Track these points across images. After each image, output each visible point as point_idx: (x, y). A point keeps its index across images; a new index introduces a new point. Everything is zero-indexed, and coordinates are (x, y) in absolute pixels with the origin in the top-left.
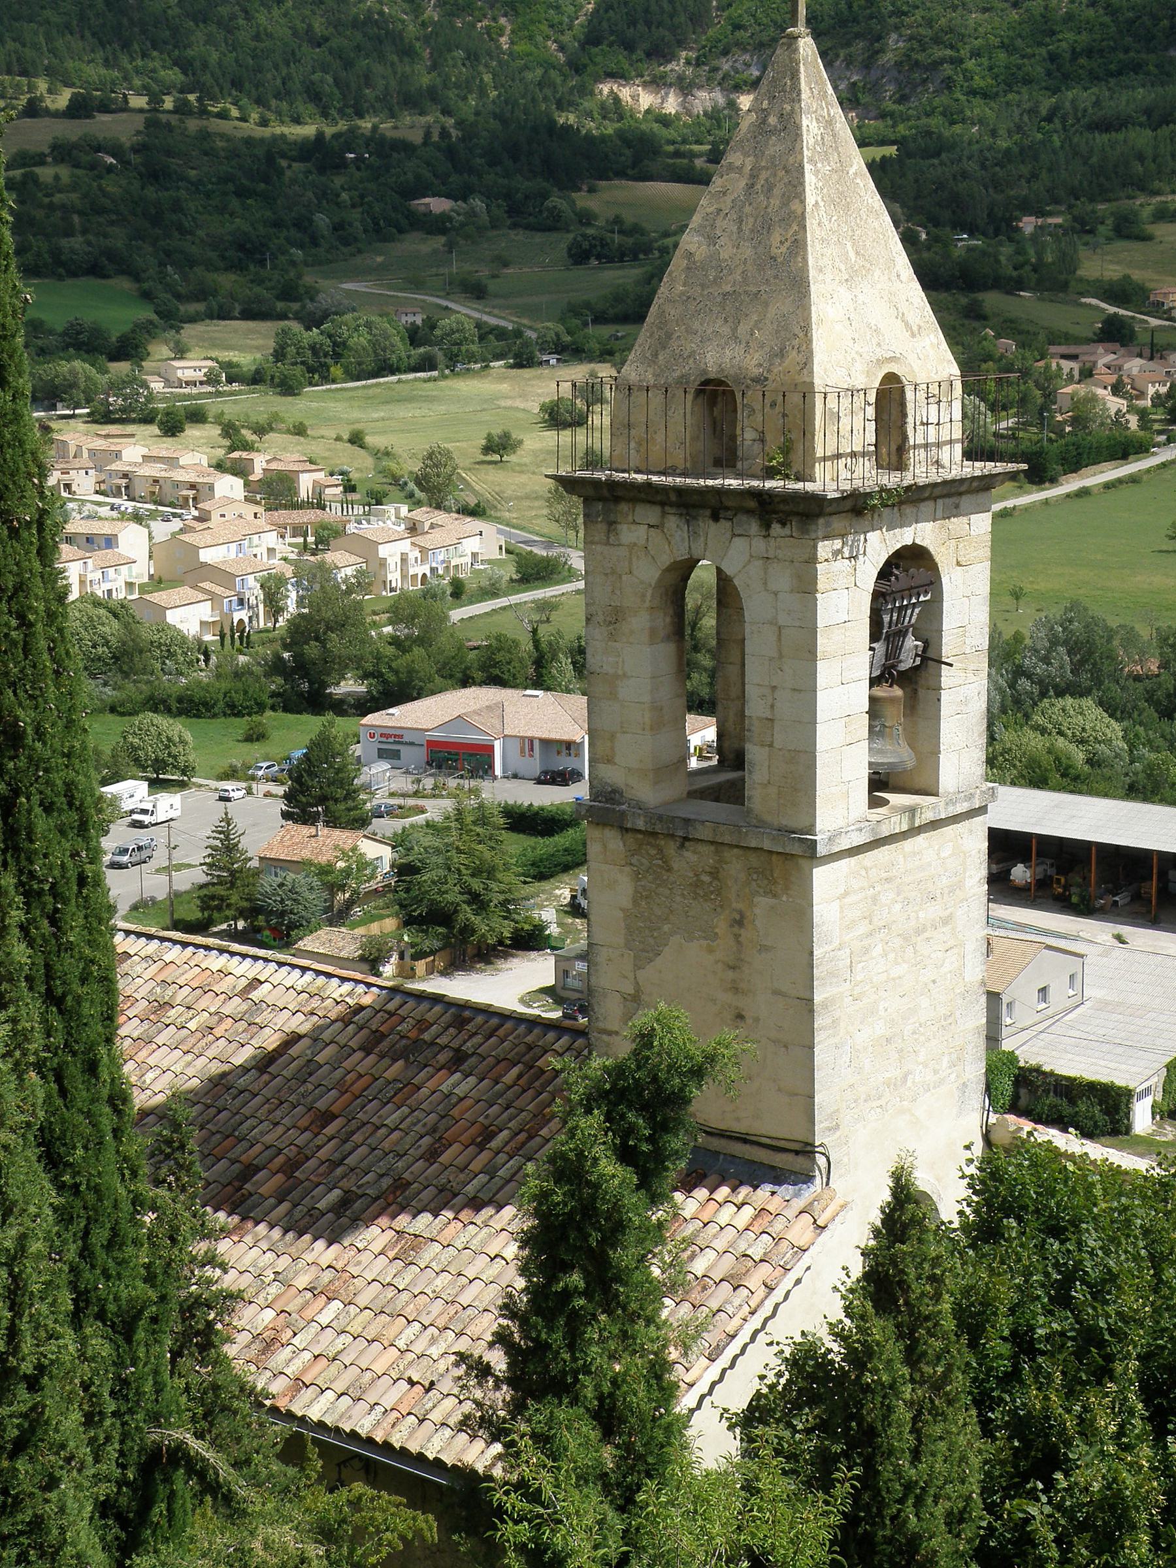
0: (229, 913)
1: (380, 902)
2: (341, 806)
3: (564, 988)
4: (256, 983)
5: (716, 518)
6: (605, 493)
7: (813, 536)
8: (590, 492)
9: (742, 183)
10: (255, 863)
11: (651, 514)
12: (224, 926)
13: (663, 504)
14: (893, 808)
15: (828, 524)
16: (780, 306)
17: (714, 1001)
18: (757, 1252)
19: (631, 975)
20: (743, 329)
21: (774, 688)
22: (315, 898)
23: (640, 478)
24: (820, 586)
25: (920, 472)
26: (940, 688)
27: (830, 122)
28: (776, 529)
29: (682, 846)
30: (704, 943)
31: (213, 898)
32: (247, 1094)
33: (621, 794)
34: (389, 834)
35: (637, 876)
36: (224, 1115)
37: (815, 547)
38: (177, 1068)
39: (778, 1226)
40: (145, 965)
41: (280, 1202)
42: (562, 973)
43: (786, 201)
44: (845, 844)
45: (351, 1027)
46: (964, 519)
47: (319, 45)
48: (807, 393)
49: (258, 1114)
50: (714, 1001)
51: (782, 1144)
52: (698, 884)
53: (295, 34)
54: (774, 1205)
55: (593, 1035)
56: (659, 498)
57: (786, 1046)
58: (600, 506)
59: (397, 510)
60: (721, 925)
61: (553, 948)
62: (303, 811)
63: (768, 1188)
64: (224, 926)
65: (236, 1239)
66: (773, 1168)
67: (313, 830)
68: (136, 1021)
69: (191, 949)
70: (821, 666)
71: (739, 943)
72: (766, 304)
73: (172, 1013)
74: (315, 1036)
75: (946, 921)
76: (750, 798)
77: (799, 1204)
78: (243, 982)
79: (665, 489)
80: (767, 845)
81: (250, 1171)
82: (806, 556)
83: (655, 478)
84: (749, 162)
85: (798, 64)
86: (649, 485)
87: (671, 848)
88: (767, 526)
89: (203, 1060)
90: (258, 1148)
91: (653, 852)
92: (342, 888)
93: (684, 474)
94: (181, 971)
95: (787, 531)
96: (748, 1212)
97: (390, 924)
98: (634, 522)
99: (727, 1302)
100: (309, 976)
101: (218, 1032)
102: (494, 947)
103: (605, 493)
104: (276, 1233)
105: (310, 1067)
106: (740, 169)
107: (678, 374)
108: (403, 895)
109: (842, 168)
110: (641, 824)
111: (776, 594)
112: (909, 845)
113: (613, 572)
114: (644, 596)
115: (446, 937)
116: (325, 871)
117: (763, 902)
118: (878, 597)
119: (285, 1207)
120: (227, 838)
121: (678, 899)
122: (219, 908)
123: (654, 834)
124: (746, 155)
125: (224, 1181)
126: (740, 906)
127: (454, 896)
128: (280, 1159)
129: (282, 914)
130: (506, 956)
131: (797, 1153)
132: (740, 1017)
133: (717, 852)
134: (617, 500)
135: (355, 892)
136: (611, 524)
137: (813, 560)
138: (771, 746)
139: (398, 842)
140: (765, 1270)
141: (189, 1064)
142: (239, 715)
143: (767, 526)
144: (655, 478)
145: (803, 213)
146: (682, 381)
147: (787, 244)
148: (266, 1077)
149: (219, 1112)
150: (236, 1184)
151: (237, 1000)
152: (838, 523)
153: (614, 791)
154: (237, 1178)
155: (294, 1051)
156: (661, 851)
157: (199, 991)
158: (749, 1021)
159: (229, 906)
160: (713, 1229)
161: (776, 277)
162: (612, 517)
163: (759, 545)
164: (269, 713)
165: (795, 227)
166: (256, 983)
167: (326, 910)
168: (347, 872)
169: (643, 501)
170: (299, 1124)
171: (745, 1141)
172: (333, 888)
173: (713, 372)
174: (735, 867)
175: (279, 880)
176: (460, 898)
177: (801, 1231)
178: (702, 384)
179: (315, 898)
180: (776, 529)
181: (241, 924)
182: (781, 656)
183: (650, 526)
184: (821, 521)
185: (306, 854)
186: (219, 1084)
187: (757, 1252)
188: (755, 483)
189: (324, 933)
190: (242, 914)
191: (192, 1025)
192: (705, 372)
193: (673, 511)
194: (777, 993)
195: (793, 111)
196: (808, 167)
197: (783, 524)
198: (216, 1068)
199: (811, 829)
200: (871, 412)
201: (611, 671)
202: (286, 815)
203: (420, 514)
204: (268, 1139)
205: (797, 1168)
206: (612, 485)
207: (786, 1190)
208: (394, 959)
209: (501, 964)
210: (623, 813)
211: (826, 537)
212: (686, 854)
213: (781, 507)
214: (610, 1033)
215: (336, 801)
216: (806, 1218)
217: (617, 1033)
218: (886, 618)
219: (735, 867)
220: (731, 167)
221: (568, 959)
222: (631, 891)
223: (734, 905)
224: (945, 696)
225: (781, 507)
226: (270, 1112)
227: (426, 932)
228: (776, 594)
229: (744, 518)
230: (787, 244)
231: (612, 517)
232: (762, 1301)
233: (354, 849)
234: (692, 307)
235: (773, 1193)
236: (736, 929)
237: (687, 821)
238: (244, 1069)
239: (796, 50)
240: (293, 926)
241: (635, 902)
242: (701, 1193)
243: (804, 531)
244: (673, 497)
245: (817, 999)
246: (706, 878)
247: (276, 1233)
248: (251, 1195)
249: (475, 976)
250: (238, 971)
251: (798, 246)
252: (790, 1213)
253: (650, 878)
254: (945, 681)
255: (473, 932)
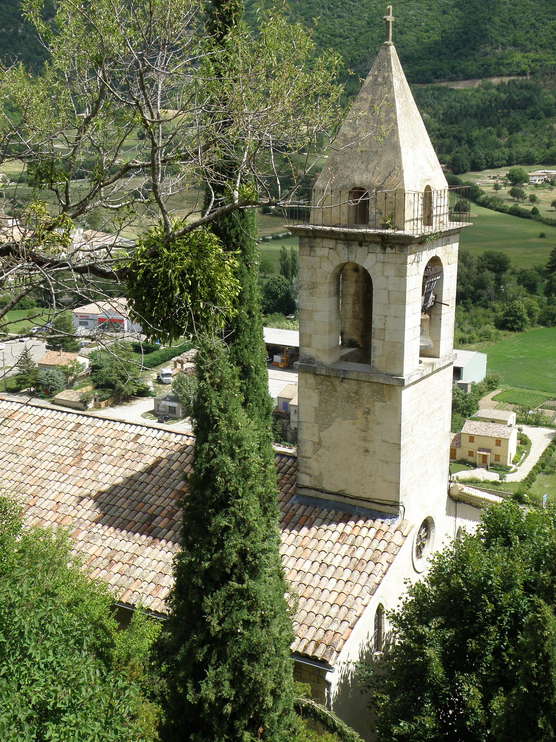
0: (29, 385)
1: (86, 380)
2: (69, 344)
3: (158, 411)
4: (139, 436)
5: (361, 245)
6: (311, 234)
7: (406, 253)
8: (303, 234)
9: (368, 106)
10: (37, 366)
11: (332, 243)
12: (26, 390)
13: (336, 239)
14: (425, 364)
15: (411, 248)
16: (387, 157)
17: (355, 445)
18: (382, 547)
19: (317, 434)
20: (371, 166)
21: (386, 316)
22: (61, 379)
23: (328, 228)
24: (408, 274)
25: (435, 227)
26: (441, 314)
27: (402, 81)
28: (388, 250)
29: (342, 381)
30: (351, 421)
31: (21, 379)
32: (144, 484)
33: (314, 360)
34: (87, 354)
35: (321, 394)
36: (136, 493)
37: (406, 258)
38: (112, 473)
39: (388, 537)
40: (88, 428)
41: (169, 530)
42: (157, 405)
43: (388, 113)
44: (413, 380)
45: (184, 454)
46: (450, 245)
47: (40, 55)
48: (403, 193)
49: (170, 496)
50: (355, 445)
51: (385, 502)
52: (349, 397)
53: (30, 50)
54: (384, 527)
55: (299, 459)
56: (336, 237)
57: (387, 463)
58: (307, 240)
59: (79, 231)
60: (359, 414)
61: (152, 396)
62: (54, 346)
63: (380, 520)
64: (26, 390)
65: (153, 546)
66: (380, 512)
67: (59, 353)
68: (89, 453)
69: (107, 422)
70: (407, 307)
71: (367, 421)
72: (381, 156)
73: (105, 449)
74: (169, 458)
75: (440, 408)
76: (373, 361)
77: (394, 527)
78: (133, 436)
79: (339, 233)
80: (382, 381)
81: (152, 517)
82: (402, 262)
83: (334, 228)
84: (370, 97)
85: (390, 56)
86: (332, 231)
87: (337, 382)
88: (384, 248)
89: (122, 470)
90: (154, 507)
91: (328, 384)
92: (71, 375)
93: (344, 227)
94: (105, 431)
95: (394, 251)
96: (373, 531)
97: (89, 388)
98: (323, 247)
99: (374, 570)
100: (161, 432)
101: (127, 457)
102: (130, 396)
103: (311, 234)
104: (170, 544)
105: (170, 472)
106: (366, 100)
107: (341, 185)
108: (95, 377)
109: (407, 101)
110: (324, 372)
111: (387, 277)
112: (430, 378)
113: (312, 267)
114: (326, 277)
115: (112, 393)
116: (65, 367)
117: (378, 405)
118: (425, 277)
119: (171, 532)
120: (26, 357)
121: (340, 403)
122: (24, 383)
123: (329, 376)
124: (368, 94)
125: (142, 521)
126: (368, 406)
127: (115, 377)
128: (165, 512)
129: (49, 385)
130: (134, 399)
131: (391, 506)
132: (367, 451)
133: (358, 384)
134: (315, 237)
135: (75, 376)
136: (312, 248)
137: (405, 263)
138: (384, 340)
139: (91, 356)
140: (386, 556)
141: (116, 471)
142: (24, 309)
143: (384, 248)
144: (334, 228)
145: (396, 119)
146: (344, 187)
147: (389, 131)
148: (151, 476)
149: (134, 491)
150: (148, 523)
151: (132, 443)
152: (414, 247)
153: (310, 359)
154: (147, 520)
155: (161, 465)
156: (332, 383)
157: (114, 440)
158: (371, 453)
159: (28, 382)
160: (360, 538)
161: (385, 145)
162: (312, 245)
163: (381, 257)
164: (36, 308)
165: (392, 124)
166: (139, 436)
167: (66, 383)
168: (72, 369)
169: (327, 238)
170: (170, 496)
171: (368, 501)
172: (67, 374)
173: (358, 184)
174: (366, 390)
175: (46, 372)
176: (117, 378)
177: (397, 539)
178: (353, 189)
179: (61, 379)
180: (388, 250)
181: (32, 389)
182: (389, 303)
183: (330, 248)
184: (409, 247)
185: (56, 362)
186: (131, 480)
187: (382, 547)
188: (379, 231)
189: (65, 392)
190: (33, 385)
191: (115, 454)
192: (354, 184)
193: (341, 242)
194: (384, 441)
195: (389, 75)
196: (396, 99)
197: (392, 248)
198: (129, 473)
199: (401, 374)
200: (421, 201)
201: (311, 309)
202: (47, 348)
203: (88, 232)
204: (158, 503)
205: (391, 512)
206: (314, 231)
207: (388, 521)
208: (93, 401)
209: (133, 402)
210: (316, 368)
211: (411, 254)
212: (343, 384)
213: (393, 241)
214: (307, 458)
215: (67, 342)
216: (398, 533)
217: (310, 458)
218: (426, 287)
219: (366, 390)
220: (362, 99)
221: (159, 400)
222: (318, 400)
223: (365, 406)
224: (443, 317)
225: (393, 241)
226: (156, 491)
227: (104, 391)
228: (387, 277)
229: (374, 245)
230: (389, 131)
231: (312, 245)
232: (387, 569)
233: (75, 360)
234: (347, 156)
235: (382, 523)
236: (366, 415)
237: (345, 371)
238: (141, 473)
239: (389, 51)
240: (53, 390)
241: (320, 404)
242: (352, 523)
243: (402, 251)
244: (342, 237)
245: (402, 443)
246: (353, 395)
247: (170, 544)
248: (155, 527)
249: (123, 407)
250: (130, 431)
251: (394, 132)
252: (392, 530)
253: (327, 394)
254: (443, 312)
255: (123, 390)
